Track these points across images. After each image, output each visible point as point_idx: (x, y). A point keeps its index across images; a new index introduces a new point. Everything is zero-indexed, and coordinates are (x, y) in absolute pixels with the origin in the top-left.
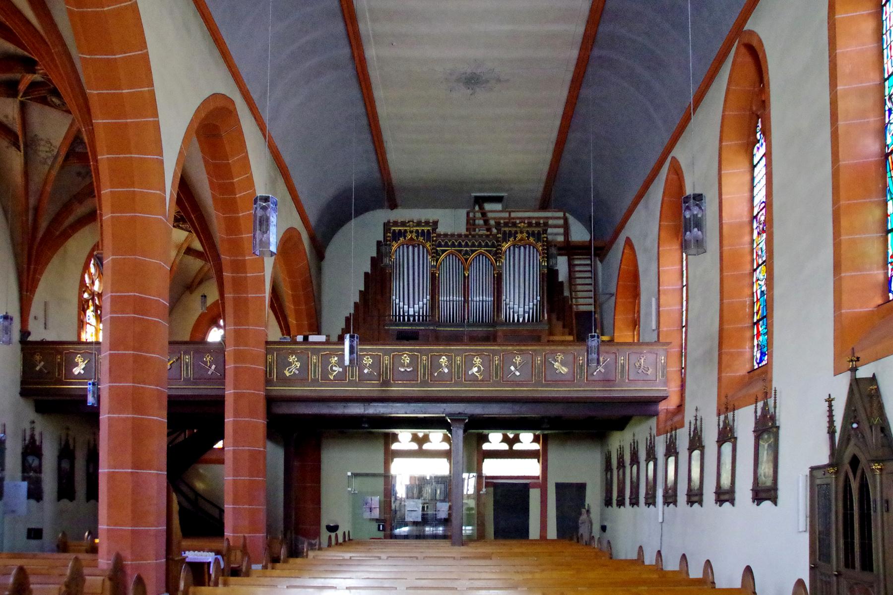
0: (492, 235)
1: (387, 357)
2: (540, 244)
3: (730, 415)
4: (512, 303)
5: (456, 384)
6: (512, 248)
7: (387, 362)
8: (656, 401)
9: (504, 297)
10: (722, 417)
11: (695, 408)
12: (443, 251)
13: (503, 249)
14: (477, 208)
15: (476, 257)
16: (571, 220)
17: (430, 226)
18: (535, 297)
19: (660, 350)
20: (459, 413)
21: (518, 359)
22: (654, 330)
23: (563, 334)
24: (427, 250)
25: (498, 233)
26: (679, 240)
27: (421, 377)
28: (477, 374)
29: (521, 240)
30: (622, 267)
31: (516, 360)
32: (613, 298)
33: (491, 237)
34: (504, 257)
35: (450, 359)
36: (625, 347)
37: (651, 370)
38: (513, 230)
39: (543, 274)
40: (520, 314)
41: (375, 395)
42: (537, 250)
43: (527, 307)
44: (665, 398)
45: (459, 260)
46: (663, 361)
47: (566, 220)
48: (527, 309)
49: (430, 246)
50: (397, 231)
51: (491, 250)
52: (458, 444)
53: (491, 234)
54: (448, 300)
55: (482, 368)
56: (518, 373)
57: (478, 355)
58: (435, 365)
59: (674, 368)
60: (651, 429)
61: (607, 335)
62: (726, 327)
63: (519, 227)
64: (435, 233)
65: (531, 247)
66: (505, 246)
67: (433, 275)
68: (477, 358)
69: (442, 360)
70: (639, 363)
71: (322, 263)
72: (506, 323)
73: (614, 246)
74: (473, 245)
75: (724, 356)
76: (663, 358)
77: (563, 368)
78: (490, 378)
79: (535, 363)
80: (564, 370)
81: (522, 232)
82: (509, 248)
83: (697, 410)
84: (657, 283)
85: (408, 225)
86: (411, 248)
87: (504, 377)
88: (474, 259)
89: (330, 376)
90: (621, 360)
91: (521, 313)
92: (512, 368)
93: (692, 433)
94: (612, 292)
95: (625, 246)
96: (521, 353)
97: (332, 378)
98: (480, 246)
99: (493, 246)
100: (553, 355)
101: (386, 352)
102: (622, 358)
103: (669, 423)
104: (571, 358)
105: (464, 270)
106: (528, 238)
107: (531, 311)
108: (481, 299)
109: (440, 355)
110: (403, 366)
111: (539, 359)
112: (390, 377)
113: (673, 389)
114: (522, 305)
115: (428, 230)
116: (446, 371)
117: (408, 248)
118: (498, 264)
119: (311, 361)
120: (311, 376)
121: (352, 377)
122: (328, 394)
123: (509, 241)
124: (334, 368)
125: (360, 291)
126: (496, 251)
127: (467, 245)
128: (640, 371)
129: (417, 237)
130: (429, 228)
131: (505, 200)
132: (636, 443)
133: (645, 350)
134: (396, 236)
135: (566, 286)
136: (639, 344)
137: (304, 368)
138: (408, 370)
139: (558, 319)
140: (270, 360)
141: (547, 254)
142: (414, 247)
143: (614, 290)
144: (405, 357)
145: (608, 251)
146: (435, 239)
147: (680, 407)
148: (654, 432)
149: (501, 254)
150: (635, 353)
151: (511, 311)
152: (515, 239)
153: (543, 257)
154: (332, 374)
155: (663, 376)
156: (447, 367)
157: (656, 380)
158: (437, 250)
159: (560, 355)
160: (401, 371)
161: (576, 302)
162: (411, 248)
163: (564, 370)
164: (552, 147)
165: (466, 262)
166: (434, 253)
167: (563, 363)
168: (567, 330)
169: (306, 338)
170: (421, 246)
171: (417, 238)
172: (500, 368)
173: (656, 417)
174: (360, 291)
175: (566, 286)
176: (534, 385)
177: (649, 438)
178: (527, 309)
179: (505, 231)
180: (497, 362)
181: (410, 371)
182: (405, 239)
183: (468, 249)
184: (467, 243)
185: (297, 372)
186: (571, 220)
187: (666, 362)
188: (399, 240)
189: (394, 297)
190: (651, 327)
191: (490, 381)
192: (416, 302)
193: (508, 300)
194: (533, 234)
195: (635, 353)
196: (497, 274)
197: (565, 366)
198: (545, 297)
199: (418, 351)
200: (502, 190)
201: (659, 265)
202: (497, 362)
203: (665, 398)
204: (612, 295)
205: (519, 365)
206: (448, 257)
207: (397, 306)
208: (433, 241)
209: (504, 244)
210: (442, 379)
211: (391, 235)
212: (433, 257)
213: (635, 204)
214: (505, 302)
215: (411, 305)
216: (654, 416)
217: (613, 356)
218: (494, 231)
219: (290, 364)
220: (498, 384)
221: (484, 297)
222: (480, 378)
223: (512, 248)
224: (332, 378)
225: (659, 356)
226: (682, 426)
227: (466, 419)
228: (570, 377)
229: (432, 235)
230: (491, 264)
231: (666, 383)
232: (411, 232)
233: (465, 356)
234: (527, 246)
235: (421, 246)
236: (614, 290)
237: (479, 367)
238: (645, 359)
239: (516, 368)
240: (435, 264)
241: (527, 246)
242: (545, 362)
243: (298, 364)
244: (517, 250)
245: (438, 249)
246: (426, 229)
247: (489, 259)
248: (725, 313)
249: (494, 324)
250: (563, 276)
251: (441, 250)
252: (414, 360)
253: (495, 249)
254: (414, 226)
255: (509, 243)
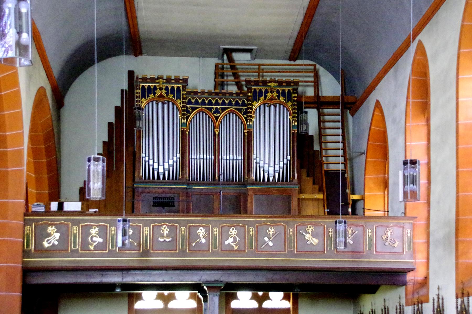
0: (243, 94)
1: (147, 228)
2: (290, 103)
3: (465, 299)
4: (262, 163)
5: (213, 254)
6: (262, 106)
7: (146, 232)
8: (403, 272)
9: (254, 157)
10: (459, 300)
11: (437, 287)
12: (194, 109)
13: (254, 108)
14: (225, 57)
15: (226, 115)
16: (322, 71)
17: (180, 83)
18: (285, 157)
19: (407, 224)
20: (215, 281)
21: (271, 231)
22: (401, 202)
23: (313, 193)
24: (177, 108)
25: (249, 92)
26: (426, 116)
27: (179, 247)
28: (233, 244)
29: (271, 99)
30: (372, 127)
31: (269, 231)
32: (364, 157)
33: (241, 95)
34: (254, 116)
35: (207, 230)
36: (372, 220)
37: (397, 243)
38: (263, 89)
39: (293, 134)
40: (270, 173)
41: (135, 265)
42: (287, 110)
43: (277, 167)
44: (412, 270)
45: (209, 117)
46: (409, 235)
47: (315, 66)
48: (277, 168)
49: (180, 103)
50: (146, 87)
51: (242, 109)
52: (213, 310)
53: (241, 93)
54: (198, 158)
55: (238, 239)
56: (271, 244)
57: (233, 226)
58: (193, 236)
59: (420, 240)
60: (400, 298)
61: (359, 194)
62: (461, 217)
63: (270, 86)
64: (185, 91)
65: (282, 106)
66: (255, 105)
67: (183, 133)
68: (233, 229)
69: (199, 231)
70: (386, 236)
71: (61, 110)
72: (257, 182)
73: (365, 104)
74: (223, 103)
75: (460, 245)
76: (409, 231)
77: (314, 239)
78: (245, 249)
79: (288, 234)
80: (315, 241)
81: (272, 92)
82: (260, 106)
83: (439, 288)
84: (404, 150)
85: (157, 81)
86: (160, 104)
87: (259, 247)
88: (224, 118)
89: (90, 246)
90: (369, 232)
91: (271, 172)
92: (266, 239)
93: (435, 310)
94: (363, 151)
95: (375, 108)
96: (274, 224)
97: (92, 248)
98: (230, 104)
99: (243, 104)
100: (304, 227)
101: (146, 224)
102: (370, 231)
103: (416, 296)
104: (320, 230)
105: (214, 128)
106: (279, 97)
107: (281, 170)
108: (231, 157)
109: (198, 226)
110: (162, 236)
111: (291, 230)
112: (150, 248)
113: (420, 258)
114: (272, 164)
115: (178, 87)
116: (203, 241)
117: (157, 104)
118: (248, 123)
119: (71, 231)
120: (71, 247)
121: (113, 247)
122: (87, 265)
123: (259, 100)
124: (94, 239)
125: (104, 143)
126: (246, 109)
127: (217, 103)
128: (387, 244)
129: (167, 94)
130: (179, 85)
131: (254, 52)
132: (387, 310)
133: (392, 223)
134: (145, 92)
135: (316, 139)
136: (388, 218)
137: (64, 239)
138: (167, 240)
139: (308, 176)
140: (28, 232)
141: (297, 117)
142: (163, 103)
143: (364, 149)
144: (165, 228)
145: (358, 108)
146: (185, 96)
147: (425, 283)
148: (403, 302)
149: (251, 112)
150: (382, 226)
151: (262, 170)
152: (265, 97)
153: (293, 117)
154: (91, 245)
155: (409, 249)
156: (204, 237)
157: (403, 252)
158: (187, 108)
159: (310, 227)
160: (160, 241)
161: (326, 153)
162: (160, 104)
163: (315, 241)
164: (303, 12)
165: (217, 119)
166: (183, 111)
167: (313, 235)
168: (317, 187)
169: (61, 206)
170: (171, 103)
171: (167, 95)
172: (255, 238)
173: (404, 287)
174: (104, 143)
175: (316, 139)
176: (286, 256)
177: (398, 307)
178: (277, 168)
179: (255, 90)
180: (251, 233)
181: (169, 242)
182: (155, 96)
183: (218, 107)
184: (217, 101)
185: (56, 243)
186: (322, 71)
187: (413, 236)
188: (148, 96)
189: (144, 155)
190: (399, 199)
191: (245, 251)
192: (166, 160)
193: (258, 160)
194: (283, 94)
195: (382, 226)
196: (247, 132)
197: (316, 238)
198: (296, 157)
199: (177, 222)
200: (253, 45)
201: (406, 140)
202: (251, 233)
203: (412, 270)
204: (363, 153)
205: (273, 235)
206: (198, 114)
207: (147, 163)
208: (183, 98)
209: (254, 103)
210: (199, 249)
211: (140, 91)
212: (183, 115)
213: (385, 71)
214: (255, 161)
215: (161, 163)
216: (403, 285)
217: (361, 228)
218: (245, 89)
219: (49, 235)
220: (252, 254)
221: (235, 156)
222: (236, 248)
223: (262, 106)
224: (92, 248)
225: (406, 230)
226: (427, 301)
227: (222, 286)
228: (320, 248)
229: (182, 93)
230: (242, 122)
231: (413, 254)
232: (161, 89)
233: (222, 227)
234: (278, 105)
235: (171, 103)
236: (364, 149)
237: (235, 238)
238: (392, 233)
239: (269, 239)
240: (185, 122)
241: (278, 105)
242: (297, 233)
243: (57, 235)
244: (267, 109)
245: (188, 106)
246: (176, 86)
247: (239, 118)
248: (460, 203)
249: (244, 183)
250: (313, 129)
251: (191, 107)
252: (173, 230)
253: (245, 107)
254: (163, 83)
255: (259, 102)
